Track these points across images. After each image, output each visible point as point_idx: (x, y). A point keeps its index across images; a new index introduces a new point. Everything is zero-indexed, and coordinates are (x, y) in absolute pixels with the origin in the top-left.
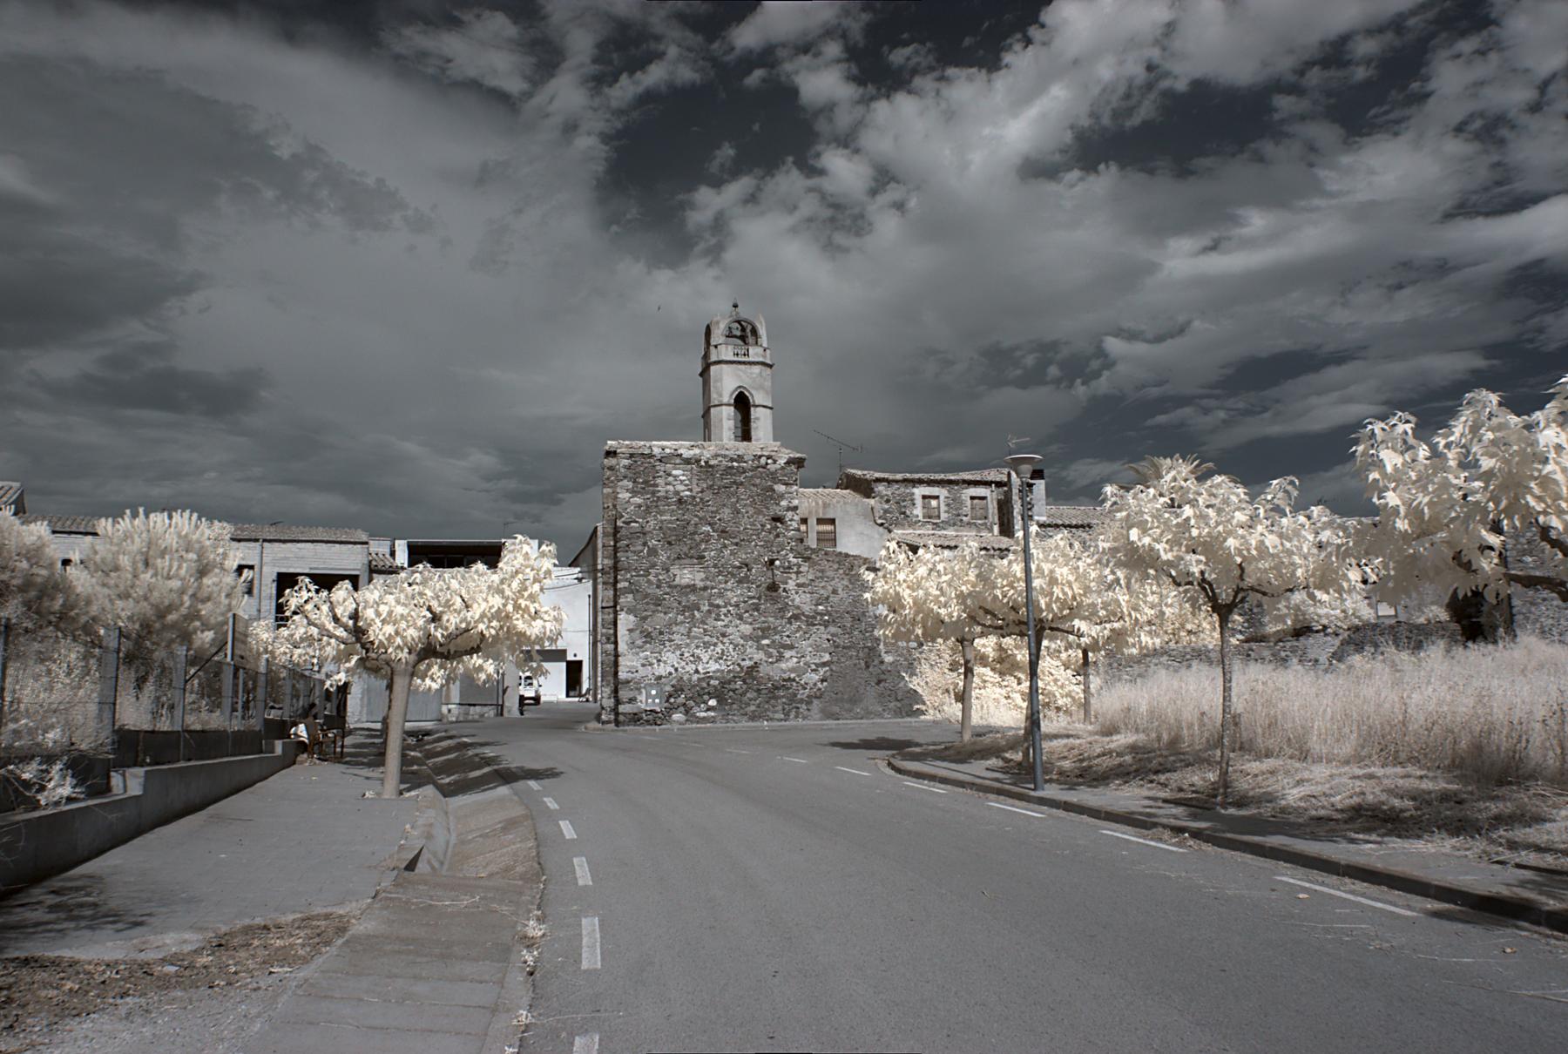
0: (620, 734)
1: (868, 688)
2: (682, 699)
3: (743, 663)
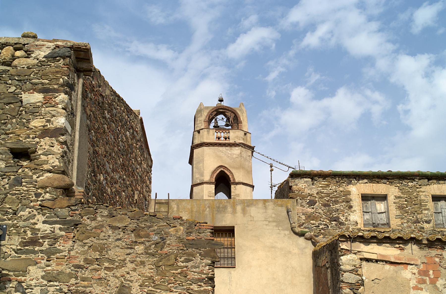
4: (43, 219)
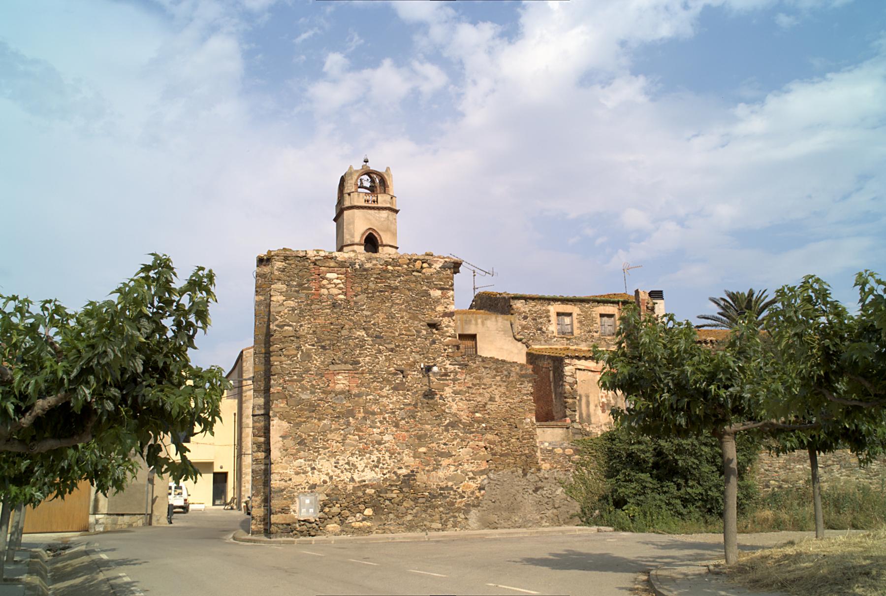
0: (274, 546)
1: (526, 496)
2: (336, 509)
3: (399, 472)
4: (449, 362)
